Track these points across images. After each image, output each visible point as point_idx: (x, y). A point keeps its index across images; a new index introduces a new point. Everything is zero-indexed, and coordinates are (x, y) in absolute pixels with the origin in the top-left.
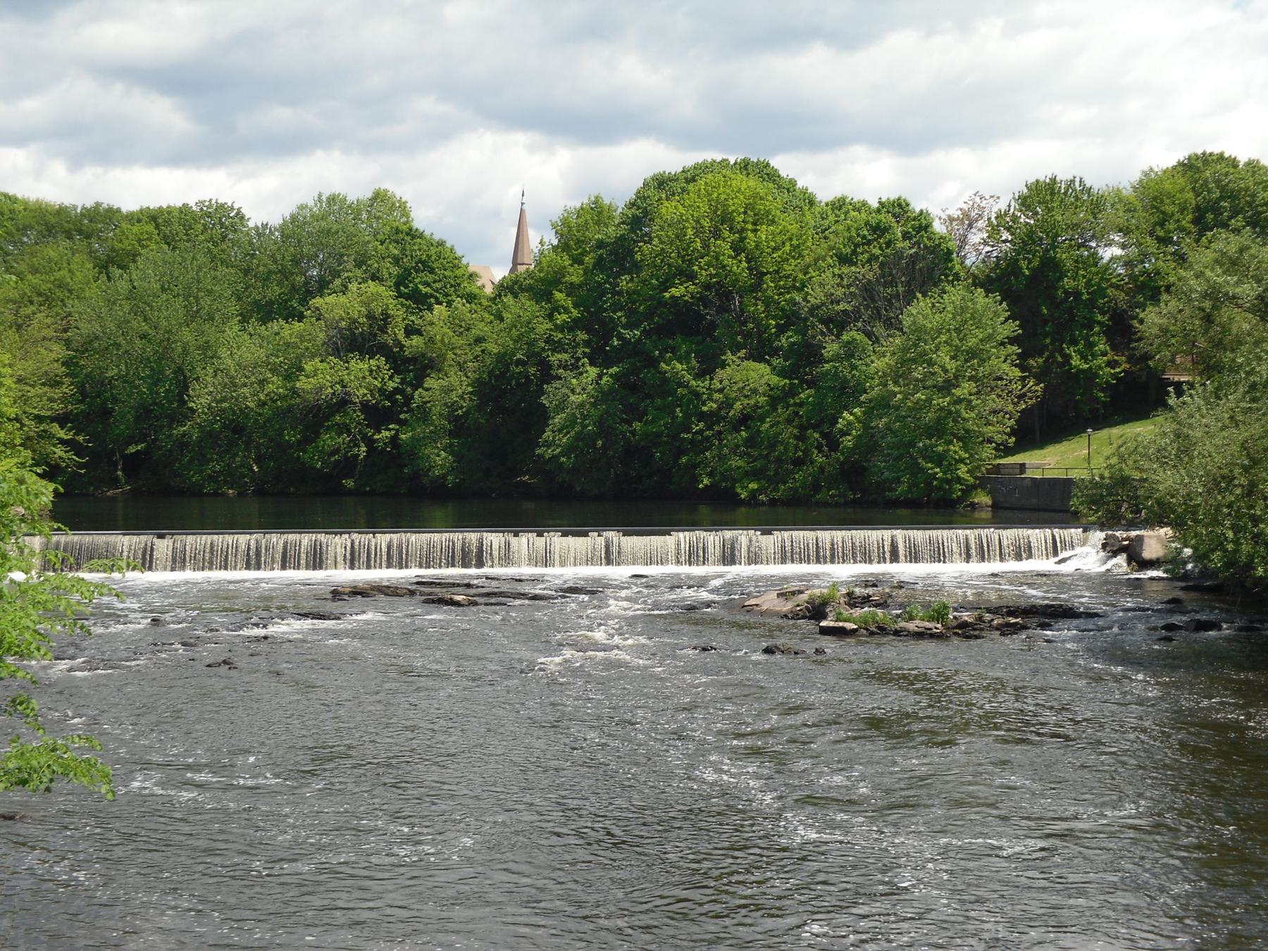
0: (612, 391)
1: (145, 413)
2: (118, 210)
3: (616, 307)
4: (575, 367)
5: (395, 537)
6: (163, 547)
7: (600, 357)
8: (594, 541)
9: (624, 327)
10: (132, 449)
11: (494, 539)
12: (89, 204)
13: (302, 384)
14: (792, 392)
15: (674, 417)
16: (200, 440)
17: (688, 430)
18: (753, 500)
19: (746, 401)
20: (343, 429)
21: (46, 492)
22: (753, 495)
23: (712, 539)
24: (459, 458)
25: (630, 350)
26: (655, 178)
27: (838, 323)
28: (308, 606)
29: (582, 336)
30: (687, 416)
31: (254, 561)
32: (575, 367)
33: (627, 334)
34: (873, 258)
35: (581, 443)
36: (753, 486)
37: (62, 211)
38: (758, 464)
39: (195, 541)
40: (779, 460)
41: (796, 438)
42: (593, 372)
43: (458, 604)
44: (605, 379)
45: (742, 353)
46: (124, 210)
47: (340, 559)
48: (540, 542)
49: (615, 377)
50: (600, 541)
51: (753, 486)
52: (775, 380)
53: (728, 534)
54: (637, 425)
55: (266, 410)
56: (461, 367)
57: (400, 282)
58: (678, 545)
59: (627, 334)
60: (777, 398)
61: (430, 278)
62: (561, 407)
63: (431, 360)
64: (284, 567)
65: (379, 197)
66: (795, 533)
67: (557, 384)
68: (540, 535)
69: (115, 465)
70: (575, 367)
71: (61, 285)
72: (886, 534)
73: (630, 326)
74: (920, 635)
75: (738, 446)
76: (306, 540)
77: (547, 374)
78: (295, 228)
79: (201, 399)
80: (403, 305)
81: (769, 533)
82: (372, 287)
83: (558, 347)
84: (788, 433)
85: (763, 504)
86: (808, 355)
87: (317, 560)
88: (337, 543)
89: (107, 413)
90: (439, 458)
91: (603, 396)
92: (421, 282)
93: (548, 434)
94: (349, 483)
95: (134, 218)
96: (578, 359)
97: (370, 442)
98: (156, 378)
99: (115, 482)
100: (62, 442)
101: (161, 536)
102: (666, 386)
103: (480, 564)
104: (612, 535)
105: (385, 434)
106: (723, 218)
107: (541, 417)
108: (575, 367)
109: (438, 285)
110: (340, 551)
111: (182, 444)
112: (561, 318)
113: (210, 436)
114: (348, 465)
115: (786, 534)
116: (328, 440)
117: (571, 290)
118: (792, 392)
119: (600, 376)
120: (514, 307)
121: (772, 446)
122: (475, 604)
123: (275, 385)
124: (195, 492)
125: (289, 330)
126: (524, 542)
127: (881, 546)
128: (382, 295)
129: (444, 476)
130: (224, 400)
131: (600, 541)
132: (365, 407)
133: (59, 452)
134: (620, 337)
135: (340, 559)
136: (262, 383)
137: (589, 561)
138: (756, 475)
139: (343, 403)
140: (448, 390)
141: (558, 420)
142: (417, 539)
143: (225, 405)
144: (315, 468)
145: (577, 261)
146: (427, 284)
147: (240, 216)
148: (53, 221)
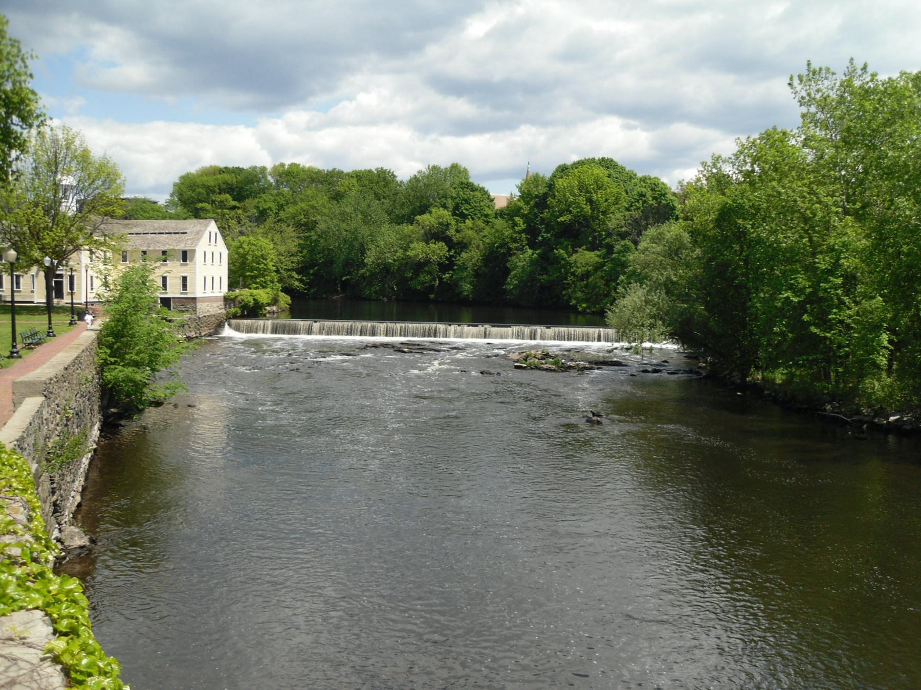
2: (342, 172)
3: (541, 224)
4: (521, 249)
5: (403, 325)
6: (316, 326)
7: (532, 245)
8: (480, 329)
9: (544, 232)
10: (344, 278)
11: (441, 327)
12: (330, 169)
14: (603, 265)
16: (370, 276)
17: (566, 279)
18: (583, 313)
19: (583, 269)
20: (429, 273)
22: (584, 309)
23: (527, 330)
24: (475, 287)
25: (545, 242)
26: (559, 167)
27: (623, 236)
28: (345, 351)
29: (523, 235)
31: (350, 332)
32: (522, 250)
33: (545, 235)
34: (638, 208)
36: (584, 305)
37: (319, 172)
38: (588, 296)
39: (328, 324)
40: (596, 294)
41: (605, 285)
42: (530, 251)
43: (404, 352)
44: (535, 255)
45: (584, 247)
46: (345, 172)
47: (382, 332)
48: (459, 328)
50: (483, 329)
51: (584, 305)
52: (597, 259)
53: (533, 328)
55: (397, 263)
56: (478, 247)
57: (457, 207)
58: (555, 333)
59: (545, 235)
61: (468, 207)
63: (466, 244)
64: (361, 335)
65: (454, 167)
66: (577, 329)
68: (459, 325)
69: (336, 284)
70: (522, 250)
71: (313, 207)
72: (597, 330)
73: (547, 232)
74: (546, 370)
75: (582, 288)
76: (369, 324)
77: (510, 253)
78: (415, 179)
79: (370, 258)
80: (454, 219)
81: (549, 328)
82: (442, 212)
83: (515, 240)
84: (601, 283)
86: (610, 249)
87: (373, 334)
88: (382, 326)
89: (332, 262)
90: (467, 287)
91: (533, 262)
92: (464, 209)
93: (509, 280)
94: (432, 296)
95: (350, 176)
96: (524, 246)
97: (441, 279)
99: (337, 293)
100: (297, 279)
101: (315, 322)
102: (557, 260)
103: (435, 336)
104: (487, 326)
105: (447, 275)
106: (583, 187)
109: (472, 210)
110: (382, 329)
112: (517, 229)
113: (373, 275)
115: (556, 329)
116: (424, 278)
117: (523, 216)
118: (603, 265)
119: (533, 254)
120: (500, 223)
122: (411, 352)
123: (400, 253)
125: (407, 228)
126: (452, 328)
128: (446, 215)
129: (468, 295)
130: (379, 259)
131: (483, 329)
132: (440, 264)
133: (297, 283)
135: (382, 332)
136: (396, 252)
137: (477, 337)
138: (586, 300)
140: (472, 257)
142: (411, 326)
143: (380, 261)
144: (417, 290)
145: (527, 203)
146: (467, 210)
147: (395, 176)
148: (315, 176)
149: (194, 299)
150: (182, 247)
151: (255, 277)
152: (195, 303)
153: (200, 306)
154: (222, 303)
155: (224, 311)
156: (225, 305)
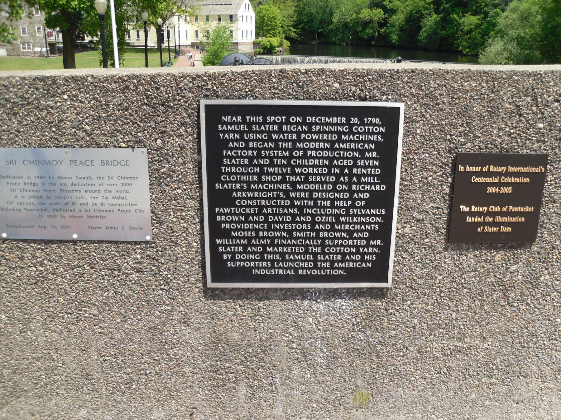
0: (439, 21)
1: (322, 22)
4: (430, 14)
7: (437, 12)
10: (319, 31)
13: (361, 16)
14: (481, 25)
15: (454, 30)
16: (336, 30)
17: (457, 34)
18: (466, 55)
20: (372, 28)
21: (287, 43)
22: (467, 52)
24: (400, 37)
30: (457, 30)
33: (445, 6)
35: (429, 37)
40: (476, 44)
42: (435, 16)
49: (440, 18)
51: (467, 50)
52: (477, 21)
54: (444, 32)
59: (445, 6)
60: (478, 26)
62: (425, 26)
67: (425, 19)
83: (426, 9)
85: (470, 55)
91: (437, 23)
93: (421, 33)
94: (373, 43)
97: (379, 32)
98: (324, 12)
99: (315, 39)
100: (294, 32)
102: (452, 21)
107: (420, 28)
108: (430, 14)
111: (331, 30)
113: (337, 29)
114: (373, 38)
116: (369, 31)
121: (474, 40)
123: (354, 15)
124: (334, 44)
127: (324, 61)
129: (395, 43)
133: (293, 34)
134: (443, 7)
136: (352, 15)
138: (469, 47)
139: (371, 21)
141: (424, 29)
149: (237, 43)
150: (230, 13)
151: (269, 30)
152: (237, 45)
153: (240, 47)
154: (252, 46)
155: (253, 51)
156: (254, 47)
